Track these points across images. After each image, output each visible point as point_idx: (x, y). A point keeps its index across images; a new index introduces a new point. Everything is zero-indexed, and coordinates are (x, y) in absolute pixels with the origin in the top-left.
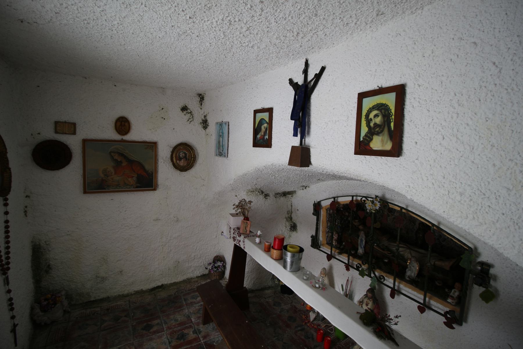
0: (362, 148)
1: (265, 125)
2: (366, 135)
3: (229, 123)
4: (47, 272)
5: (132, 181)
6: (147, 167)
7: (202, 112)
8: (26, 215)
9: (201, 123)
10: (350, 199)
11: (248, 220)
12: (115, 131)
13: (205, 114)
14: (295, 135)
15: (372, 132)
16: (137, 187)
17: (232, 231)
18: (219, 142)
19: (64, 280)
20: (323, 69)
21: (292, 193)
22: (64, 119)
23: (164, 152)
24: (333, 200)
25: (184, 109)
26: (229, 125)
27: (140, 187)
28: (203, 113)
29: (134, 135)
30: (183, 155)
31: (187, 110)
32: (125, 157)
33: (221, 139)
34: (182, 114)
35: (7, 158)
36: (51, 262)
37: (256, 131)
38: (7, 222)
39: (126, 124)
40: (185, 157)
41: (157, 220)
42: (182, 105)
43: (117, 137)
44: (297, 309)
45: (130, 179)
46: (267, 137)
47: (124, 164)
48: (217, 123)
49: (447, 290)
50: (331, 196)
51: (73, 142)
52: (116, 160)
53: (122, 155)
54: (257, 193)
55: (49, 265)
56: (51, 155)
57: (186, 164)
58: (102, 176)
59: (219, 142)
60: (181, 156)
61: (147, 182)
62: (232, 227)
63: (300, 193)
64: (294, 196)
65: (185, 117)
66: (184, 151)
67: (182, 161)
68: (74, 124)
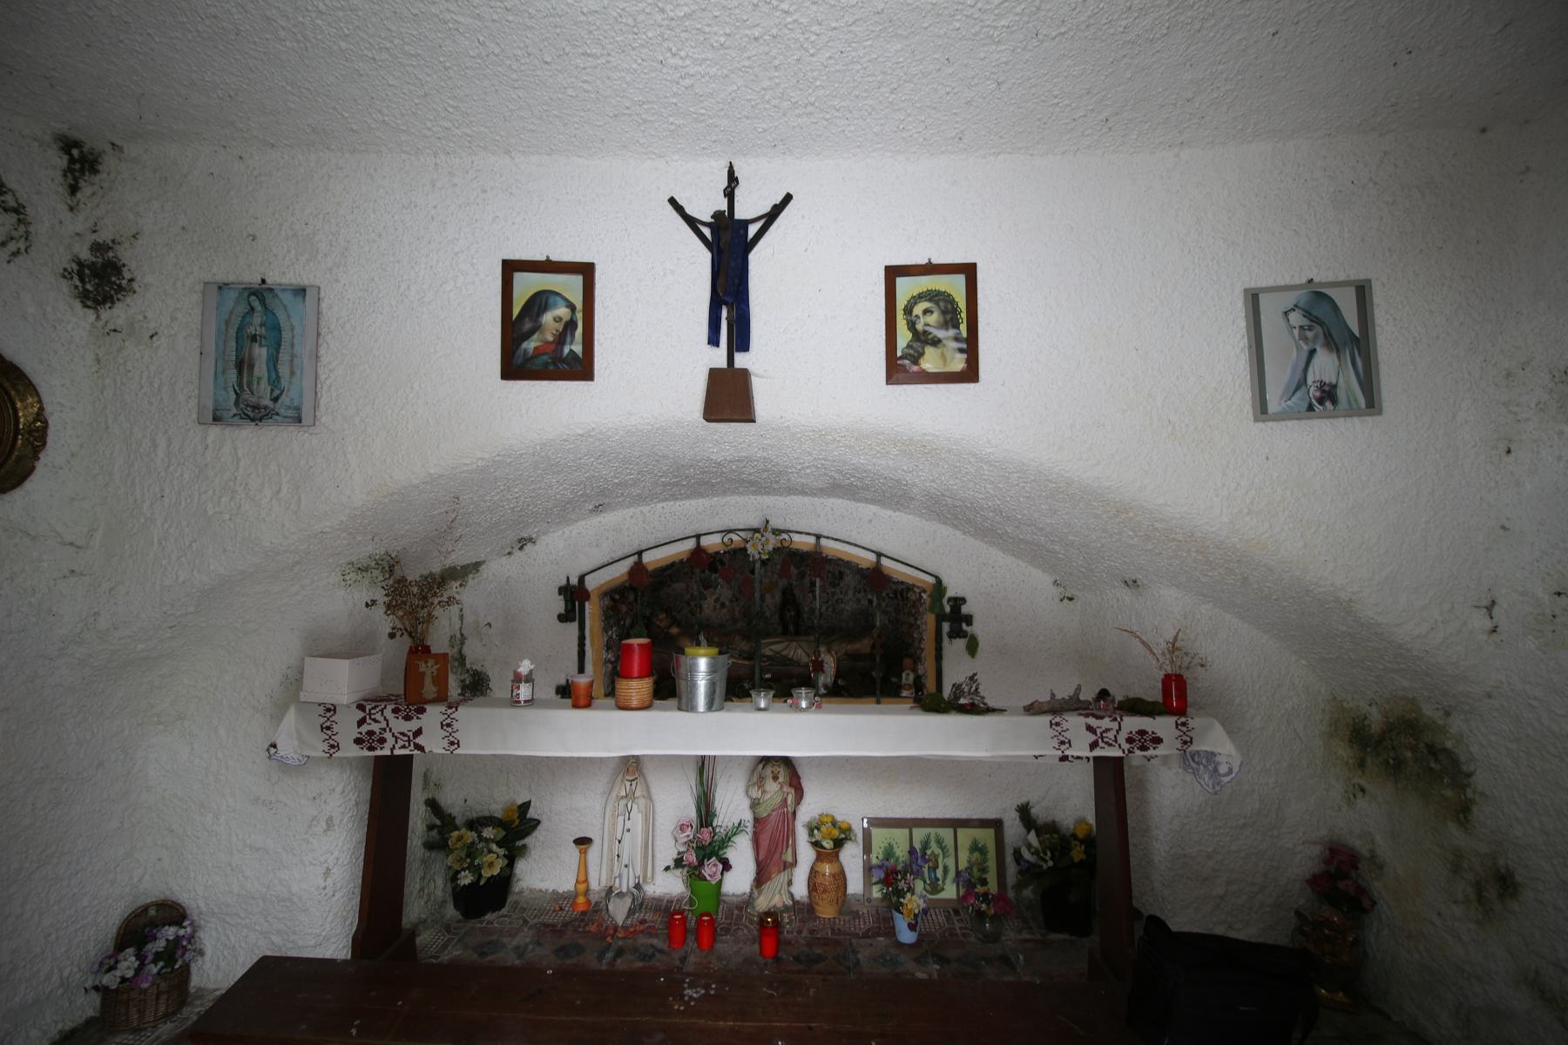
0: (899, 369)
1: (562, 312)
2: (909, 346)
7: (80, 223)
9: (66, 275)
10: (690, 544)
14: (714, 340)
15: (922, 339)
20: (788, 198)
21: (476, 566)
24: (630, 562)
33: (261, 353)
37: (514, 329)
44: (554, 926)
46: (578, 348)
49: (894, 680)
50: (690, 531)
63: (498, 569)
64: (471, 582)
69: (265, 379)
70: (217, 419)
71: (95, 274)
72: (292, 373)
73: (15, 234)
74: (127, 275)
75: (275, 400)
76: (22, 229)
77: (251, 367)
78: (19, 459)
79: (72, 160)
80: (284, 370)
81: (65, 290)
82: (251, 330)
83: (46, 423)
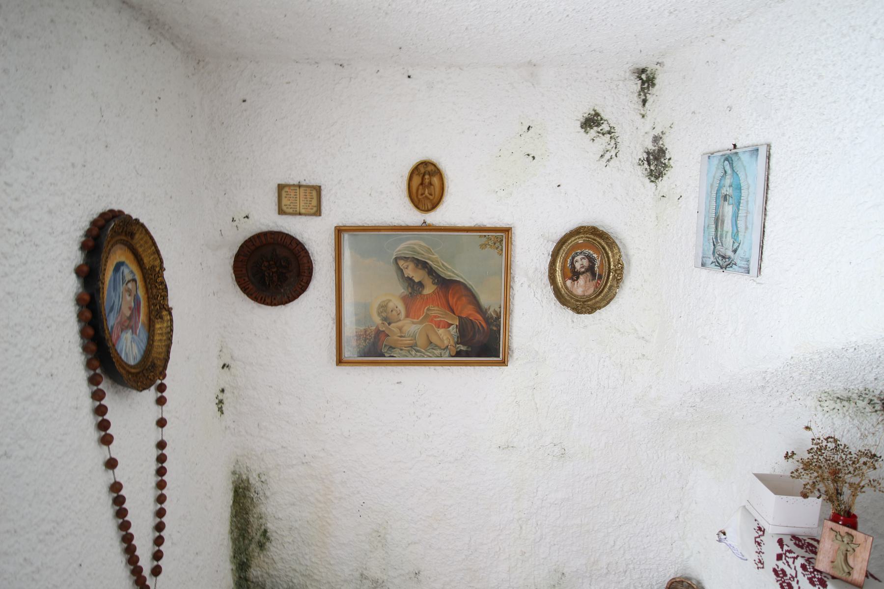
3: (769, 146)
4: (261, 546)
5: (447, 336)
6: (485, 300)
8: (221, 410)
9: (641, 162)
11: (854, 526)
12: (407, 200)
13: (657, 132)
16: (459, 354)
17: (771, 549)
18: (718, 221)
19: (295, 570)
22: (293, 178)
23: (531, 258)
25: (591, 122)
26: (768, 157)
27: (467, 354)
28: (648, 128)
29: (450, 212)
30: (586, 262)
31: (599, 125)
32: (432, 272)
34: (583, 138)
35: (163, 283)
36: (269, 525)
38: (116, 487)
39: (435, 180)
40: (591, 269)
41: (507, 447)
42: (585, 111)
43: (412, 217)
45: (441, 331)
47: (429, 289)
48: (710, 155)
51: (314, 234)
52: (410, 280)
53: (422, 265)
54: (861, 404)
55: (265, 531)
56: (271, 269)
57: (591, 291)
58: (378, 320)
59: (718, 221)
60: (578, 266)
61: (482, 342)
62: (773, 530)
65: (593, 145)
66: (587, 251)
67: (582, 280)
68: (318, 189)
69: (729, 234)
70: (703, 265)
71: (656, 159)
72: (746, 228)
73: (609, 147)
74: (668, 156)
75: (735, 251)
76: (613, 142)
77: (723, 222)
78: (611, 286)
79: (643, 83)
80: (741, 224)
81: (640, 173)
82: (723, 191)
83: (622, 265)
